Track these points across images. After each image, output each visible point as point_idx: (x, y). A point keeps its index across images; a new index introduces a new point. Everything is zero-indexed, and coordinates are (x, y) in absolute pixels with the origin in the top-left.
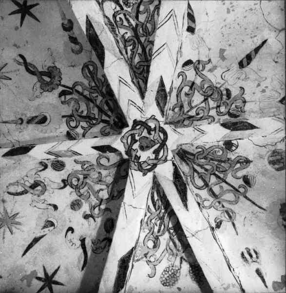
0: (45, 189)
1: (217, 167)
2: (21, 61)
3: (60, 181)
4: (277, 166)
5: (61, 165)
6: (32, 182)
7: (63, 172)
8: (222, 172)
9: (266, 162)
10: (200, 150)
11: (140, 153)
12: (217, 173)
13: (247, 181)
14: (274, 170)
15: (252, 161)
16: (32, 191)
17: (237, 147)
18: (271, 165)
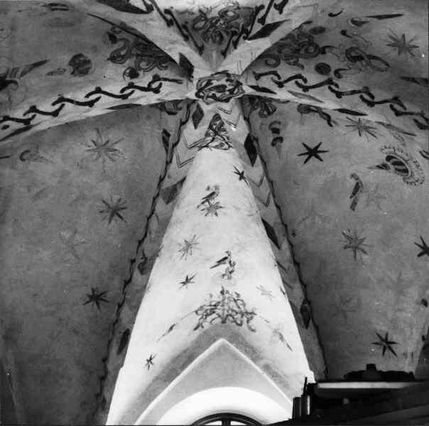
0: (348, 52)
1: (146, 48)
2: (332, 123)
3: (329, 54)
4: (82, 59)
5: (319, 68)
6: (358, 63)
7: (322, 61)
8: (140, 44)
9: (93, 62)
10: (164, 65)
11: (227, 84)
12: (146, 43)
13: (113, 39)
14: (85, 55)
15: (108, 59)
16: (363, 55)
17: (124, 73)
18: (87, 59)
